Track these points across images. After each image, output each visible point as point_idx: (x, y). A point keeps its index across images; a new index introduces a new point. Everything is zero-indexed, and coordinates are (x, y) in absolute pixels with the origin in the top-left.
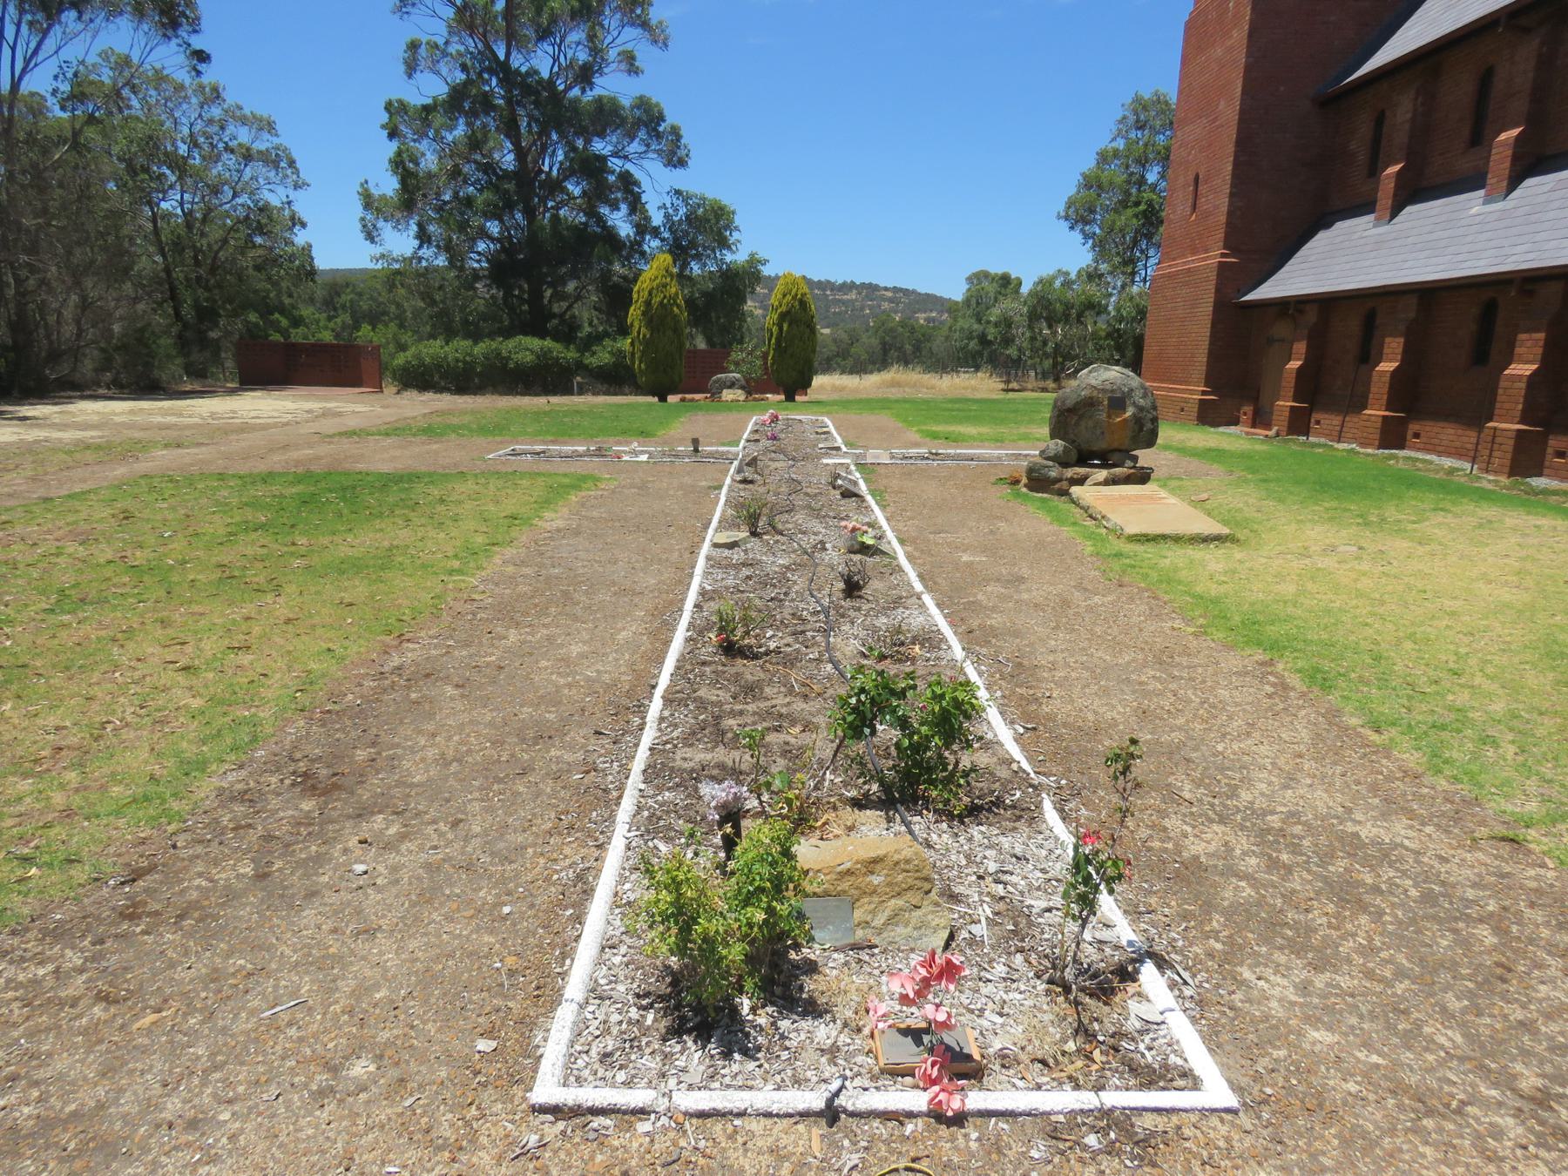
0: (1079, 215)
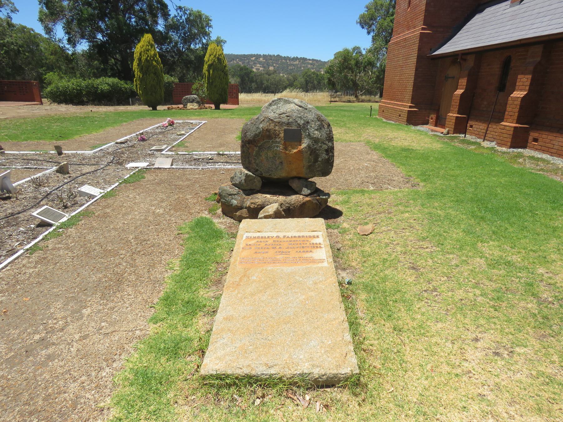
0: (366, 22)
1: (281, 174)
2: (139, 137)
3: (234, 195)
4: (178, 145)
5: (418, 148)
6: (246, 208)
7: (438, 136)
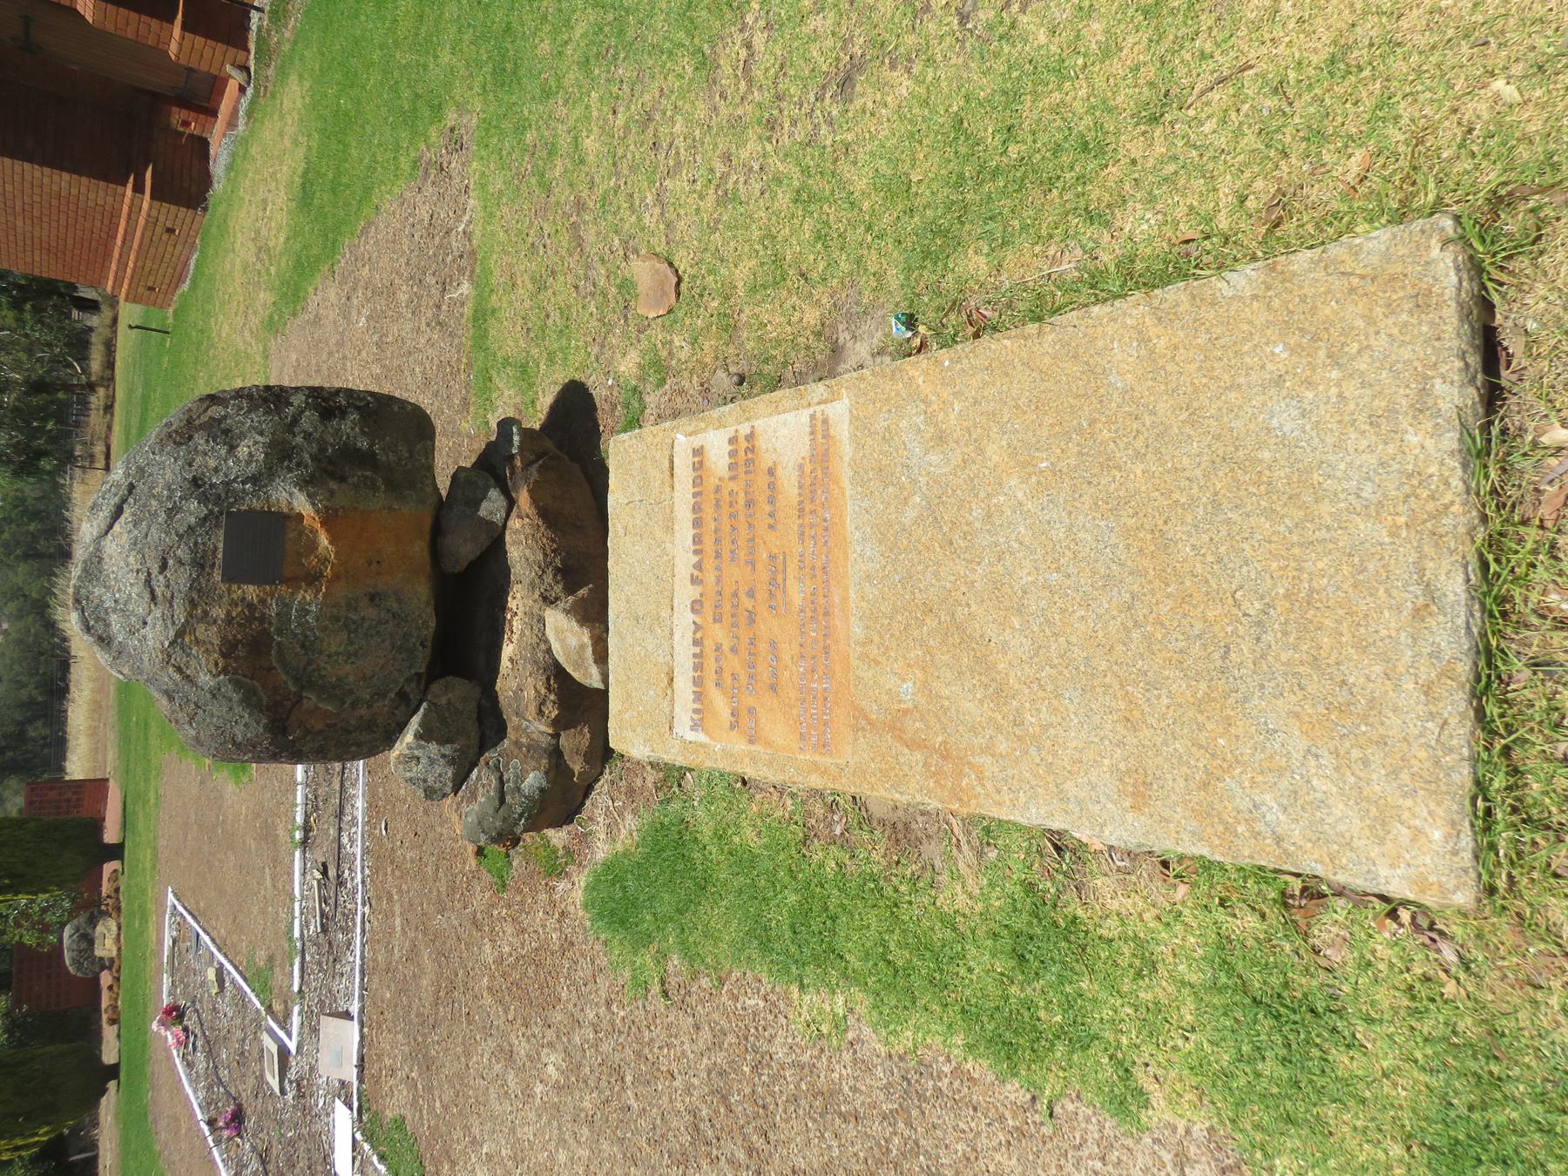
1: (419, 597)
2: (226, 1133)
3: (501, 782)
4: (263, 990)
5: (300, 153)
6: (556, 736)
7: (253, 102)
